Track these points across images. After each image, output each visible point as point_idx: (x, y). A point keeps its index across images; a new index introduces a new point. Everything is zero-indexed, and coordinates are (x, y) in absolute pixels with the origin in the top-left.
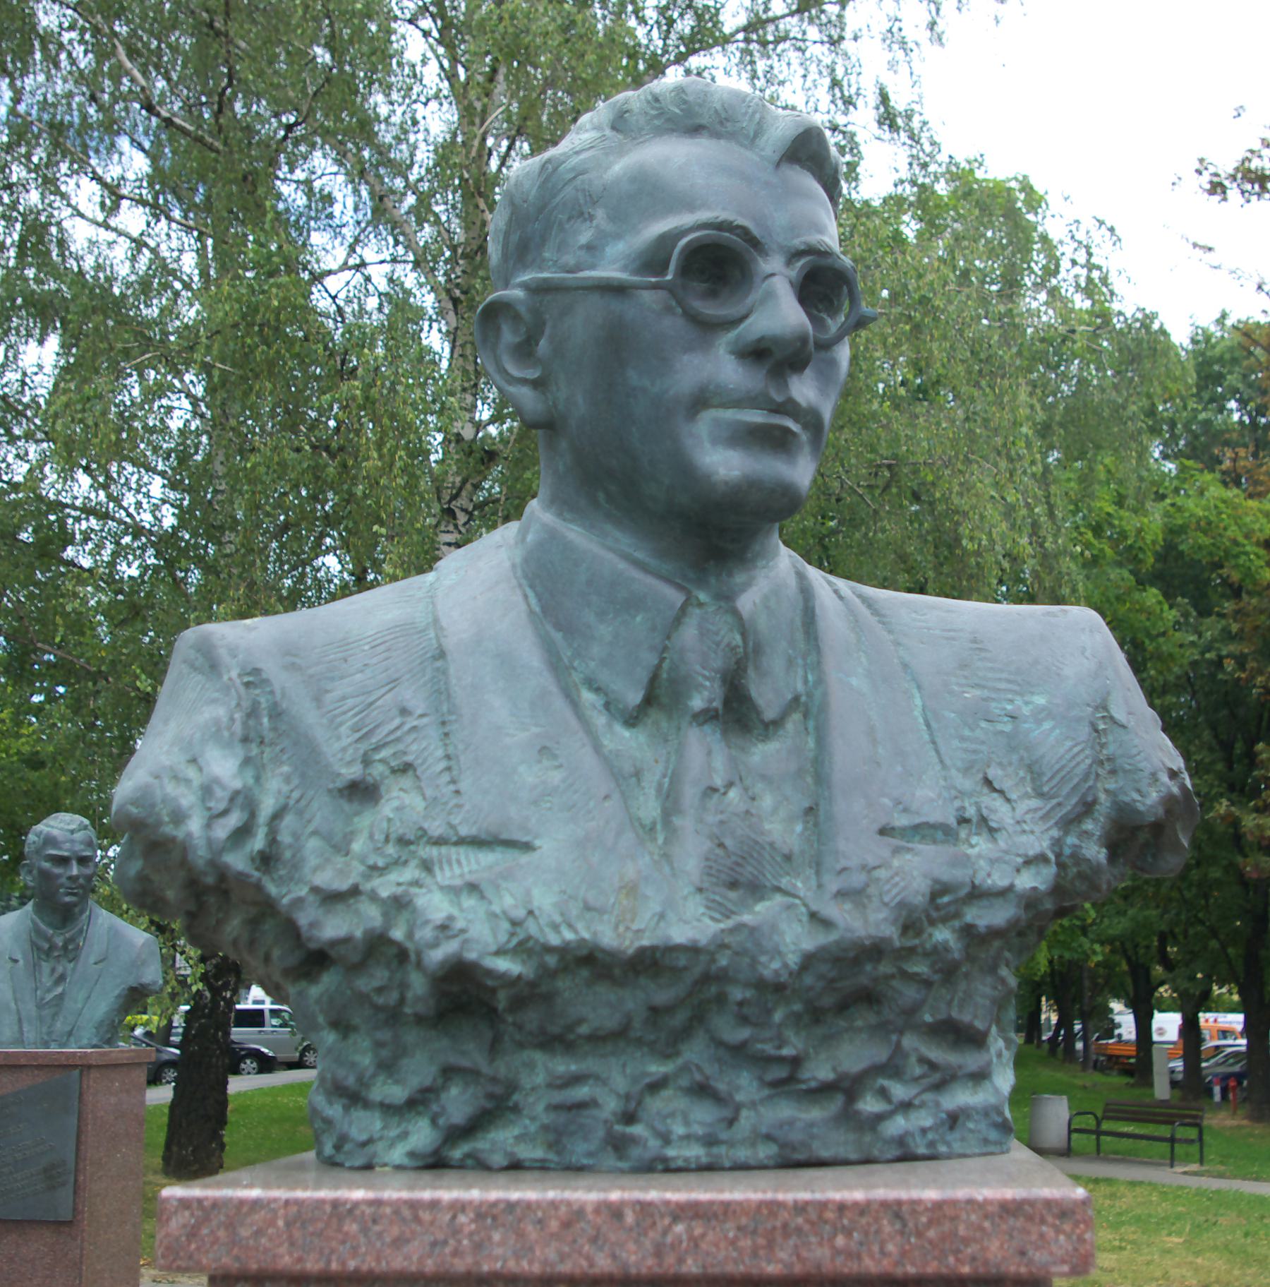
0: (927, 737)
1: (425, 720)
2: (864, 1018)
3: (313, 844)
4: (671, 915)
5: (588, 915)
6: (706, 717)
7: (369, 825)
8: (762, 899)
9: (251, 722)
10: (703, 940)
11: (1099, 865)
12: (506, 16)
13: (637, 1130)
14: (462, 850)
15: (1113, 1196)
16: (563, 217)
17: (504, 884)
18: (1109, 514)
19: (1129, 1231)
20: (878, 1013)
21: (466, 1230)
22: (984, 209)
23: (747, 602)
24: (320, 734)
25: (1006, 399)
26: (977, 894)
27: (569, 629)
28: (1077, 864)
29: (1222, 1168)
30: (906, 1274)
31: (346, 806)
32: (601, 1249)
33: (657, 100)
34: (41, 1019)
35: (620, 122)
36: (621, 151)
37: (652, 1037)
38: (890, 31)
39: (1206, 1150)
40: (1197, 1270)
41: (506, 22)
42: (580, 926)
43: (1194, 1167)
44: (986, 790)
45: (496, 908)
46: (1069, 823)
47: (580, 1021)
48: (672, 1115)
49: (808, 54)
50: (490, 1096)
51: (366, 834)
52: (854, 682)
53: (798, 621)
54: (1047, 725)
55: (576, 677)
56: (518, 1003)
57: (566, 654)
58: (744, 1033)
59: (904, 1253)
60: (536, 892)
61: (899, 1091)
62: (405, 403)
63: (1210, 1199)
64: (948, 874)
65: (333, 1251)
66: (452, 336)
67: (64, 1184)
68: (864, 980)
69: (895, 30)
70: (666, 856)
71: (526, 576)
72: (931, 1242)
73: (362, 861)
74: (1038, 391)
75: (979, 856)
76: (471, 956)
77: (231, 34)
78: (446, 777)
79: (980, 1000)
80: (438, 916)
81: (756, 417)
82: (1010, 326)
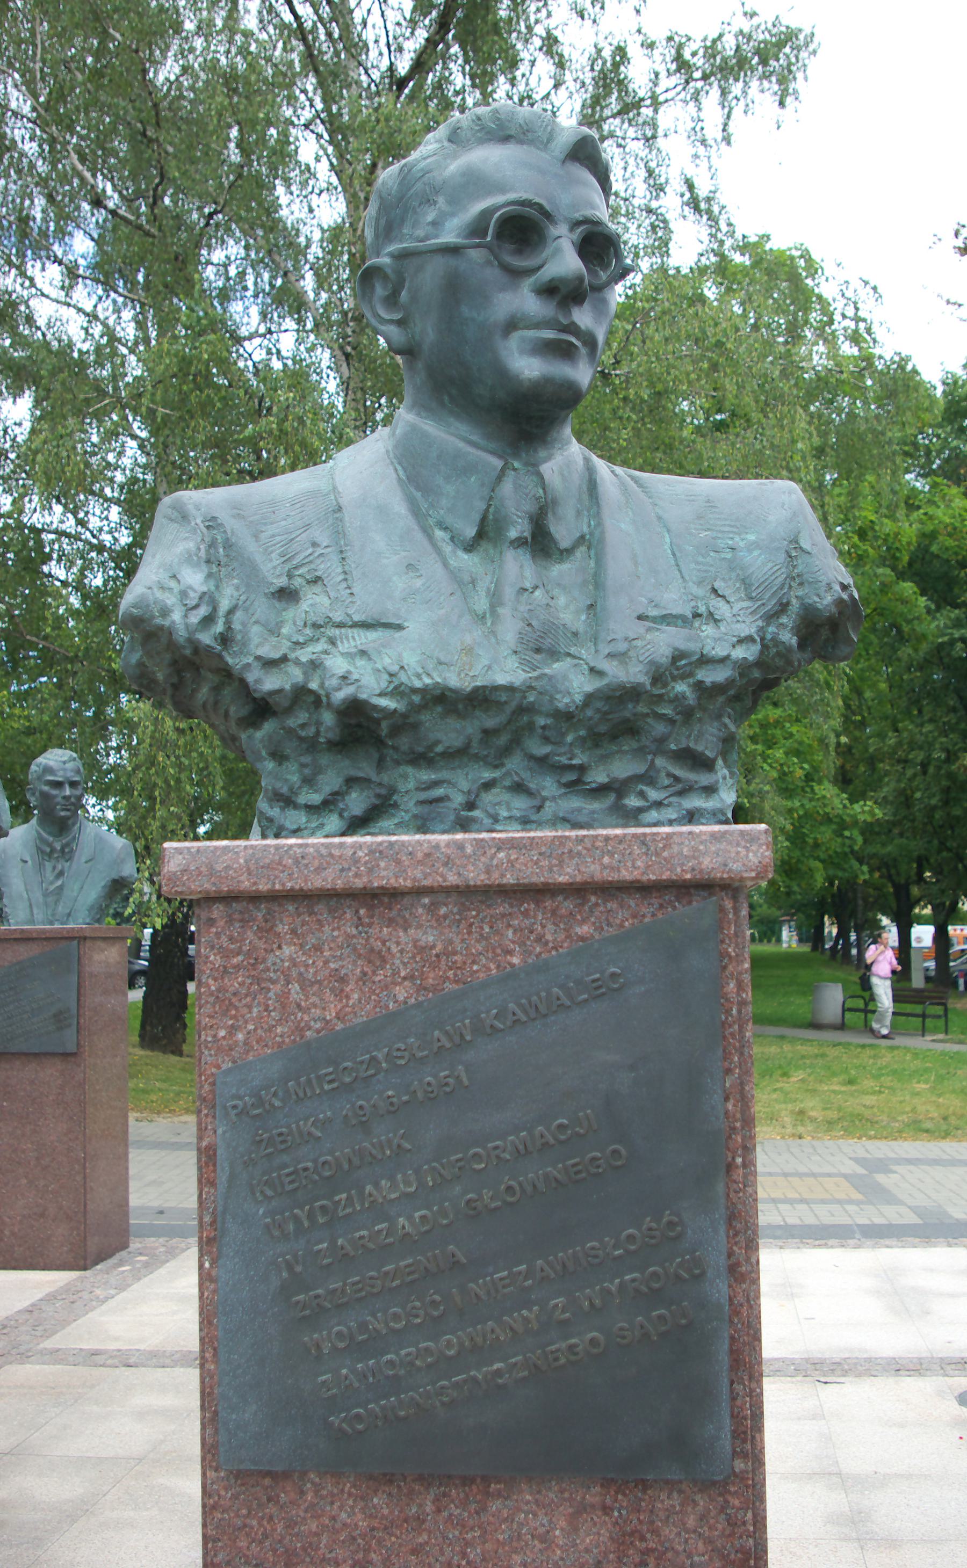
0: (673, 562)
1: (329, 550)
2: (628, 744)
3: (256, 629)
4: (495, 667)
5: (440, 667)
6: (520, 543)
7: (294, 615)
8: (558, 660)
9: (212, 551)
10: (517, 683)
11: (791, 646)
12: (382, 119)
13: (476, 813)
14: (355, 630)
15: (875, 1057)
16: (415, 204)
17: (384, 650)
18: (871, 521)
19: (887, 1080)
20: (638, 741)
21: (363, 861)
22: (769, 272)
23: (547, 469)
24: (258, 558)
25: (785, 422)
26: (705, 661)
27: (427, 489)
28: (776, 645)
29: (962, 1037)
30: (649, 880)
31: (277, 605)
32: (450, 870)
33: (479, 119)
34: (46, 904)
35: (454, 137)
36: (455, 156)
37: (485, 753)
38: (694, 129)
39: (950, 1024)
40: (938, 1106)
41: (382, 124)
42: (435, 675)
43: (941, 1036)
44: (713, 596)
45: (379, 666)
46: (770, 617)
47: (438, 742)
48: (499, 804)
49: (627, 150)
50: (378, 796)
51: (291, 622)
52: (623, 526)
53: (585, 488)
54: (756, 553)
55: (431, 522)
56: (396, 731)
57: (424, 506)
58: (547, 749)
59: (648, 867)
60: (405, 654)
61: (653, 795)
62: (312, 433)
63: (951, 1058)
64: (683, 645)
65: (276, 877)
66: (345, 385)
67: (69, 1025)
68: (627, 714)
69: (698, 129)
70: (493, 633)
71: (396, 457)
72: (665, 859)
73: (289, 640)
74: (815, 421)
75: (707, 637)
76: (363, 696)
77: (161, 139)
78: (344, 585)
79: (710, 738)
80: (340, 672)
81: (549, 334)
82: (790, 368)
